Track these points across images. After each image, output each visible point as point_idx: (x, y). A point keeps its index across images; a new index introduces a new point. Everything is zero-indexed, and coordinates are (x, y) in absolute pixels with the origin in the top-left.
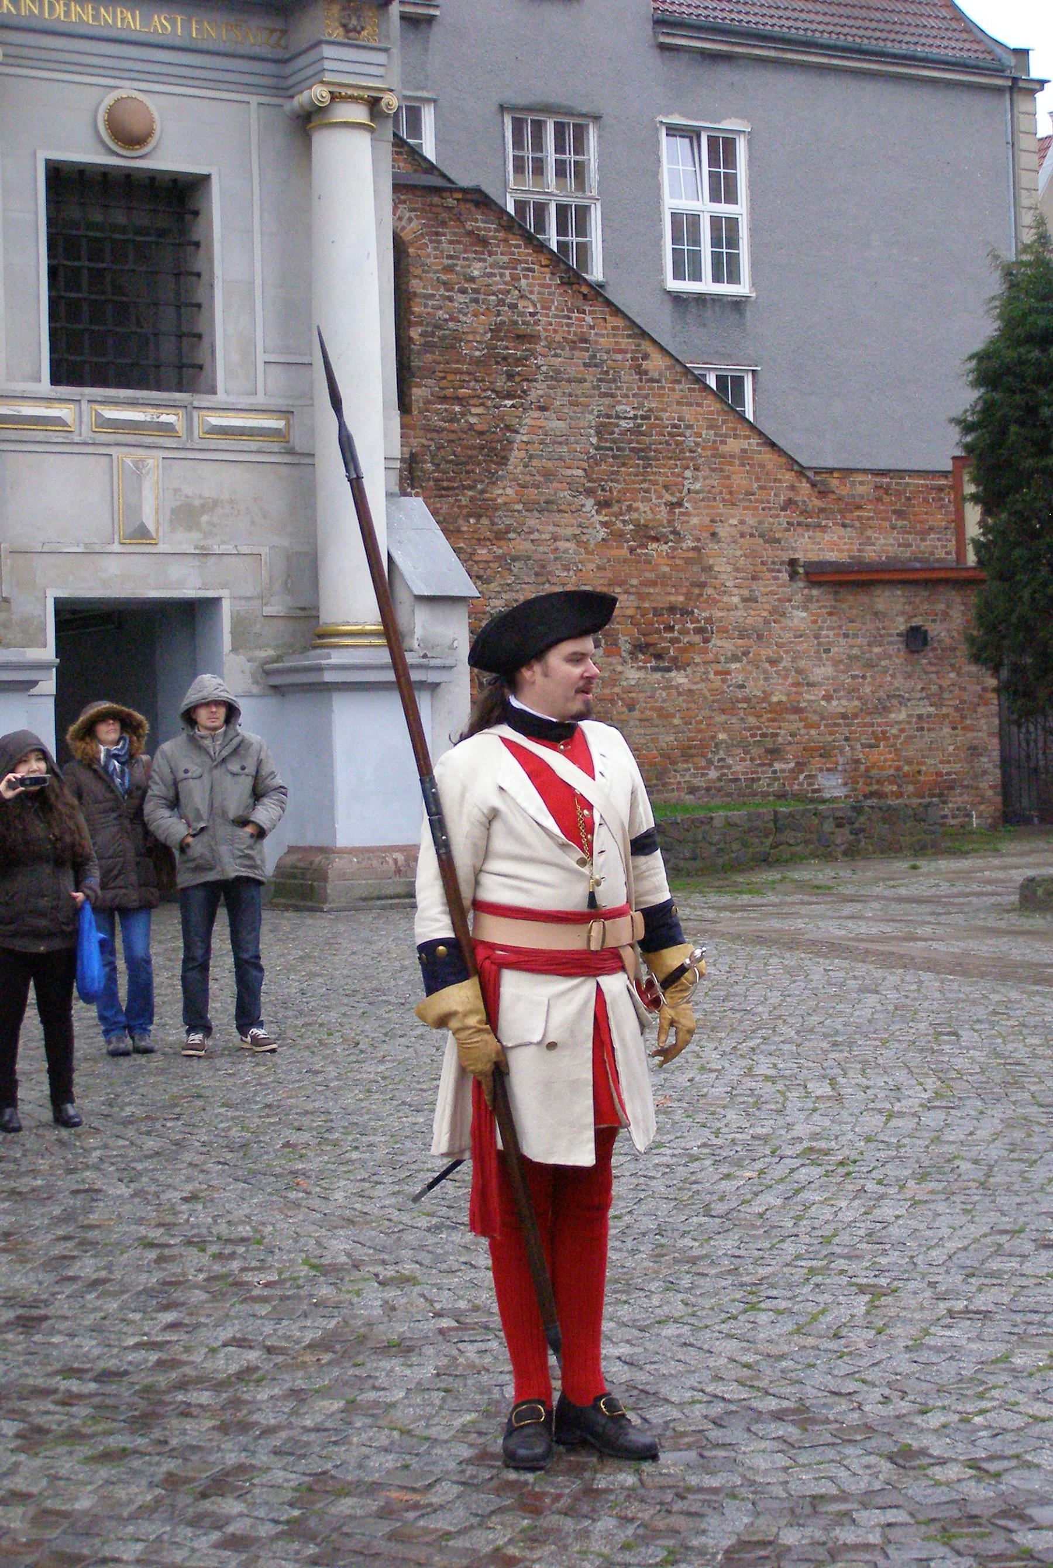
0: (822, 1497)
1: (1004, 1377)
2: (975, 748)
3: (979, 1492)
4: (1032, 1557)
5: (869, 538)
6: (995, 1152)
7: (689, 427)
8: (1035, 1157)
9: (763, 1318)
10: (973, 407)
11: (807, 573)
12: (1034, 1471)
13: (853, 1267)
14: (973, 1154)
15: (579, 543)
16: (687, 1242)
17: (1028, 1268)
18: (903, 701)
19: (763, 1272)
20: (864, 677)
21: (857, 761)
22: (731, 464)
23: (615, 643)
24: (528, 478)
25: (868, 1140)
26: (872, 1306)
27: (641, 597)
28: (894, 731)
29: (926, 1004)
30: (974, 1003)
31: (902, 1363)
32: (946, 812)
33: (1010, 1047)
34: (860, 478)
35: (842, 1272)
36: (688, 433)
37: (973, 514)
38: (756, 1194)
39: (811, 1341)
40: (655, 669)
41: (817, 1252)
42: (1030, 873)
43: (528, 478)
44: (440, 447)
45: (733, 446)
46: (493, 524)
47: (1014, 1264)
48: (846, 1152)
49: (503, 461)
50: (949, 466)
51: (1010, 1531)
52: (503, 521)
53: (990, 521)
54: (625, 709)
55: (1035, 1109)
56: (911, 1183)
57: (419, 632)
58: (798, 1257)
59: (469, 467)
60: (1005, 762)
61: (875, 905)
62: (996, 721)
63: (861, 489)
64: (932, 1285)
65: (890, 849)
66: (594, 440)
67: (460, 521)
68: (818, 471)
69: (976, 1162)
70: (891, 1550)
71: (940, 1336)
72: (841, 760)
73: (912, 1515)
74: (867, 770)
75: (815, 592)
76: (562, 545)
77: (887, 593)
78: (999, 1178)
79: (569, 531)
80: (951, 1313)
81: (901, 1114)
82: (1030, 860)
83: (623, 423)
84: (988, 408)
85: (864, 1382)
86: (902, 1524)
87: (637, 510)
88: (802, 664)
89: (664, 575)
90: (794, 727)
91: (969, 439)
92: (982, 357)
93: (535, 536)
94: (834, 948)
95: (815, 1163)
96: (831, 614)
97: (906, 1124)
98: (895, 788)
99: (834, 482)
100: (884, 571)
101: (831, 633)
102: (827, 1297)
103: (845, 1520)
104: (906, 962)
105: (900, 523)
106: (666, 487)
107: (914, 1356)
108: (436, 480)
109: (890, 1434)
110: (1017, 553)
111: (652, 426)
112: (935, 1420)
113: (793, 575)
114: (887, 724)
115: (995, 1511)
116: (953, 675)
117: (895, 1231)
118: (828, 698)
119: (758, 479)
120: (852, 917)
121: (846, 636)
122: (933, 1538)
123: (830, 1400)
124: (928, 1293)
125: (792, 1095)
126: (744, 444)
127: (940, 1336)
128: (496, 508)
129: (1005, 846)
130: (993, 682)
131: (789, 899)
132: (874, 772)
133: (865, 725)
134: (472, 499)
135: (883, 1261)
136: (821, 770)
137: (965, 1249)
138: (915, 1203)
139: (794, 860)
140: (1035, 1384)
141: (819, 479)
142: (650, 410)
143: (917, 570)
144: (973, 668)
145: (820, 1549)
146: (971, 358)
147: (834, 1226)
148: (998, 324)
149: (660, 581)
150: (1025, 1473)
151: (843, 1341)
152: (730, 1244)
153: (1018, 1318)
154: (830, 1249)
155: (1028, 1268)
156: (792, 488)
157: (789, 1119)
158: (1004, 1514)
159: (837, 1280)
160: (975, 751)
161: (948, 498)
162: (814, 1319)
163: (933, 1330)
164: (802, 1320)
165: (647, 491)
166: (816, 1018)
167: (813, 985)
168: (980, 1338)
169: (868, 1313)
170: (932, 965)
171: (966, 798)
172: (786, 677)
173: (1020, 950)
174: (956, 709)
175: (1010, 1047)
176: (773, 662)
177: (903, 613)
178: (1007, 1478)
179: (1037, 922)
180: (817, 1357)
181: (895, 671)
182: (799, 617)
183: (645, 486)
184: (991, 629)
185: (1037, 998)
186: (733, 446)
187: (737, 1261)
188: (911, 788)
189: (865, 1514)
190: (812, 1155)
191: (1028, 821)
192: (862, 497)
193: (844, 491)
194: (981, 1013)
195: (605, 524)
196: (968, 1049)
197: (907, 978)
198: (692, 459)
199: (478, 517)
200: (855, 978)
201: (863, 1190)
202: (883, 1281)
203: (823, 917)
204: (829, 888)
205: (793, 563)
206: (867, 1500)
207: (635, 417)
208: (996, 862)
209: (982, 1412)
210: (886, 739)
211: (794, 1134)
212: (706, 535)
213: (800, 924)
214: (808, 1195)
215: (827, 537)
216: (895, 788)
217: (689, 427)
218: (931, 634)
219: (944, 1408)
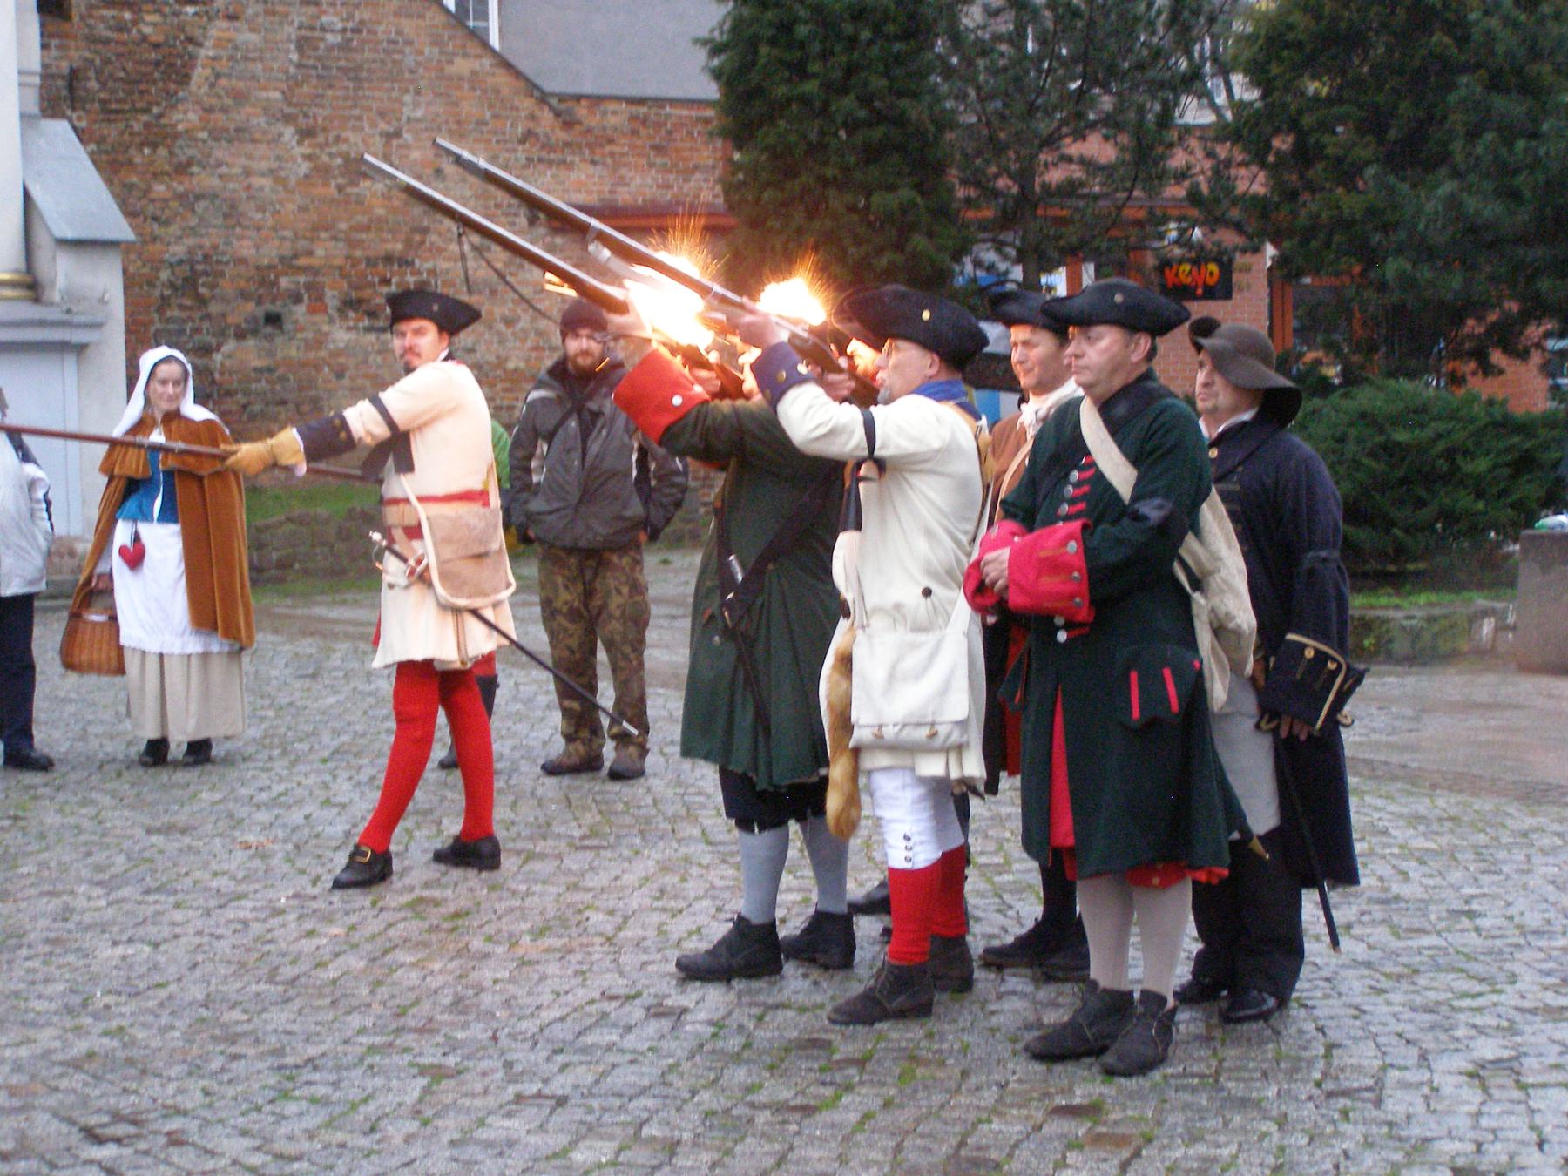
5: (622, 178)
7: (409, 43)
8: (682, 904)
9: (291, 1108)
10: (721, 25)
15: (277, 180)
16: (237, 1015)
17: (631, 1041)
19: (312, 1051)
22: (459, 88)
23: (321, 298)
24: (214, 101)
27: (352, 244)
34: (612, 106)
35: (406, 1050)
36: (408, 50)
38: (337, 955)
39: (340, 1136)
40: (368, 330)
43: (214, 101)
44: (106, 62)
45: (462, 66)
46: (171, 154)
49: (184, 79)
52: (184, 152)
53: (737, 156)
54: (332, 377)
57: (61, 282)
59: (143, 87)
63: (612, 120)
64: (508, 1065)
66: (295, 57)
67: (133, 151)
68: (562, 98)
69: (611, 913)
71: (500, 1127)
76: (257, 181)
79: (264, 165)
81: (542, 856)
83: (330, 38)
84: (738, 25)
87: (346, 140)
89: (379, 219)
91: (716, 62)
93: (224, 170)
95: (419, 916)
99: (581, 111)
102: (379, 1081)
105: (659, 160)
106: (382, 114)
107: (456, 1153)
108: (103, 102)
111: (363, 42)
117: (487, 999)
119: (491, 106)
126: (476, 65)
127: (500, 1127)
128: (176, 136)
134: (147, 125)
135: (460, 1035)
137: (562, 1019)
141: (565, 107)
142: (362, 22)
149: (375, 225)
152: (285, 1016)
154: (402, 1022)
155: (631, 1041)
156: (532, 117)
159: (396, 1059)
162: (354, 1107)
165: (359, 118)
168: (542, 1128)
169: (421, 1100)
172: (523, 341)
176: (509, 322)
183: (356, 112)
186: (462, 66)
187: (285, 1039)
193: (592, 121)
195: (308, 157)
198: (412, 81)
199: (154, 146)
207: (344, 30)
212: (430, 171)
215: (573, 176)
217: (409, 43)
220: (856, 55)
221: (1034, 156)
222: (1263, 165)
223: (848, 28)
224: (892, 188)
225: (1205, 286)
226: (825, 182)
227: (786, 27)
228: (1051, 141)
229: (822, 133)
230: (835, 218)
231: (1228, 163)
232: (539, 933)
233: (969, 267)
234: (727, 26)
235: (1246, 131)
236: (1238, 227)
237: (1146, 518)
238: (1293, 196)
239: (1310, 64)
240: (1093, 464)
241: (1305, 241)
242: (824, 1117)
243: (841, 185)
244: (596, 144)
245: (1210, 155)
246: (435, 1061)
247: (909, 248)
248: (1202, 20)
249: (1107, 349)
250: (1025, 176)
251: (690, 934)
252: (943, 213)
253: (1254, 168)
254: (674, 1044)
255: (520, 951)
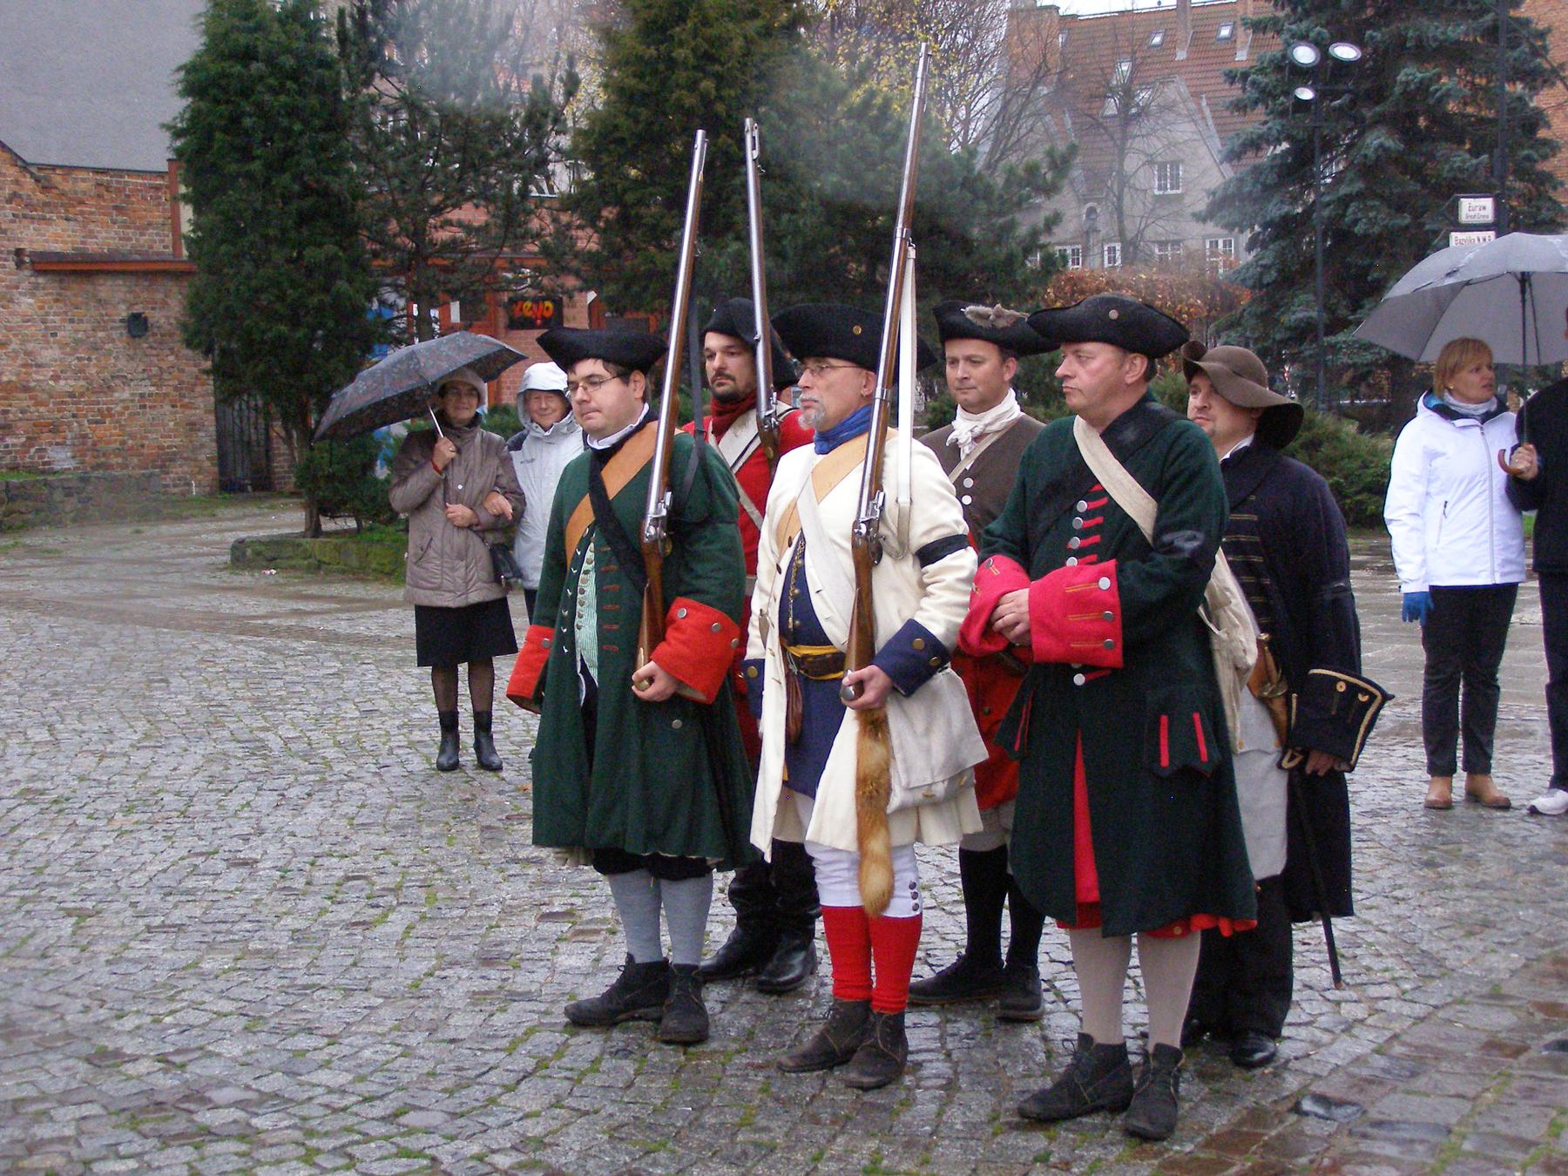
0: (23, 1100)
1: (193, 981)
2: (193, 424)
3: (166, 1082)
4: (210, 1133)
5: (91, 231)
6: (195, 784)
8: (231, 786)
10: (182, 116)
11: (33, 262)
12: (215, 1060)
13: (63, 893)
14: (177, 787)
17: (219, 884)
18: (126, 381)
20: (89, 359)
21: (85, 437)
25: (81, 779)
26: (78, 927)
28: (119, 409)
29: (140, 655)
30: (184, 652)
31: (103, 976)
32: (168, 481)
33: (214, 691)
34: (82, 175)
35: (52, 899)
37: (187, 212)
39: (19, 963)
41: (29, 882)
42: (243, 535)
47: (208, 882)
48: (60, 791)
50: (164, 167)
51: (191, 1112)
55: (233, 745)
56: (119, 816)
58: (11, 888)
60: (221, 437)
61: (100, 566)
62: (212, 399)
63: (83, 186)
64: (134, 905)
65: (117, 515)
68: (41, 167)
69: (178, 794)
70: (83, 1142)
71: (138, 950)
72: (69, 435)
73: (104, 1107)
74: (95, 444)
75: (41, 280)
77: (109, 283)
78: (198, 807)
80: (149, 929)
81: (113, 755)
82: (244, 523)
84: (195, 116)
85: (67, 995)
86: (95, 1117)
88: (30, 346)
90: (25, 404)
91: (178, 143)
92: (190, 69)
94: (60, 607)
95: (31, 802)
96: (57, 301)
97: (116, 763)
98: (120, 460)
99: (57, 178)
100: (106, 263)
101: (57, 318)
103: (44, 1118)
104: (122, 617)
105: (120, 218)
107: (114, 968)
109: (88, 1039)
110: (224, 248)
112: (129, 1023)
113: (20, 265)
114: (113, 402)
115: (179, 1096)
116: (171, 358)
117: (102, 860)
118: (56, 378)
120: (78, 578)
121: (71, 321)
122: (122, 1126)
123: (36, 1013)
124: (129, 912)
125: (13, 742)
127: (138, 950)
129: (222, 512)
130: (208, 364)
131: (20, 563)
132: (100, 446)
133: (93, 403)
135: (90, 886)
136: (51, 444)
137: (164, 871)
138: (121, 833)
139: (26, 527)
140: (220, 985)
141: (43, 175)
143: (137, 262)
144: (189, 352)
145: (19, 1146)
146: (179, 69)
147: (46, 858)
148: (204, 39)
150: (208, 1062)
151: (49, 961)
153: (208, 928)
154: (42, 879)
155: (219, 884)
157: (8, 764)
158: (186, 1098)
159: (46, 905)
160: (193, 426)
161: (164, 196)
162: (24, 942)
163: (132, 944)
164: (12, 944)
166: (38, 671)
167: (39, 640)
168: (173, 949)
169: (74, 933)
170: (150, 620)
171: (186, 468)
173: (230, 605)
174: (176, 388)
175: (214, 691)
177: (124, 301)
178: (190, 1068)
179: (246, 578)
180: (25, 977)
181: (118, 354)
182: (26, 303)
184: (202, 317)
185: (241, 647)
188: (135, 460)
189: (62, 1111)
190: (29, 795)
191: (242, 489)
192: (84, 193)
193: (66, 186)
194: (191, 661)
196: (176, 694)
197: (125, 633)
200: (77, 633)
201: (74, 824)
202: (89, 905)
203: (50, 579)
204: (57, 551)
205: (19, 252)
206: (63, 1099)
208: (213, 526)
209: (172, 1012)
210: (112, 416)
211: (12, 777)
213: (29, 585)
214: (24, 832)
215: (52, 229)
216: (120, 460)
218: (151, 320)
219: (138, 1012)
220: (290, 143)
221: (426, 221)
222: (593, 225)
223: (285, 122)
224: (320, 245)
225: (543, 318)
226: (267, 240)
227: (235, 120)
228: (437, 210)
229: (265, 202)
230: (276, 267)
231: (568, 226)
232: (129, 810)
233: (375, 305)
234: (187, 116)
235: (581, 203)
236: (577, 274)
237: (1180, 550)
238: (617, 254)
239: (631, 156)
240: (1104, 492)
241: (627, 287)
242: (379, 930)
243: (282, 242)
244: (70, 205)
245: (555, 220)
246: (78, 905)
247: (334, 289)
248: (550, 120)
249: (1098, 371)
250: (418, 234)
251: (243, 806)
252: (358, 264)
253: (590, 231)
254: (254, 885)
255: (116, 825)
